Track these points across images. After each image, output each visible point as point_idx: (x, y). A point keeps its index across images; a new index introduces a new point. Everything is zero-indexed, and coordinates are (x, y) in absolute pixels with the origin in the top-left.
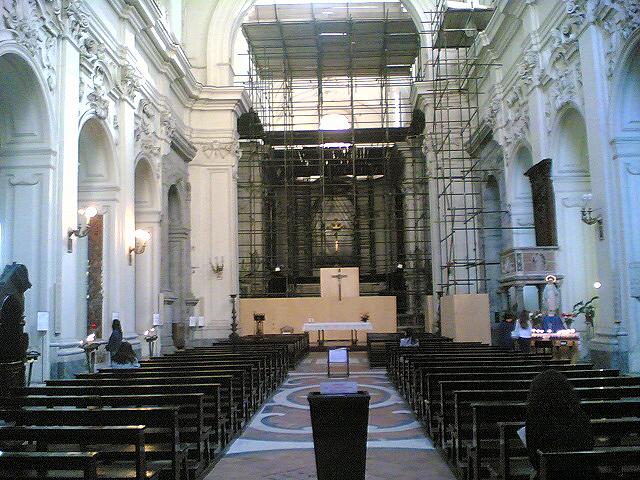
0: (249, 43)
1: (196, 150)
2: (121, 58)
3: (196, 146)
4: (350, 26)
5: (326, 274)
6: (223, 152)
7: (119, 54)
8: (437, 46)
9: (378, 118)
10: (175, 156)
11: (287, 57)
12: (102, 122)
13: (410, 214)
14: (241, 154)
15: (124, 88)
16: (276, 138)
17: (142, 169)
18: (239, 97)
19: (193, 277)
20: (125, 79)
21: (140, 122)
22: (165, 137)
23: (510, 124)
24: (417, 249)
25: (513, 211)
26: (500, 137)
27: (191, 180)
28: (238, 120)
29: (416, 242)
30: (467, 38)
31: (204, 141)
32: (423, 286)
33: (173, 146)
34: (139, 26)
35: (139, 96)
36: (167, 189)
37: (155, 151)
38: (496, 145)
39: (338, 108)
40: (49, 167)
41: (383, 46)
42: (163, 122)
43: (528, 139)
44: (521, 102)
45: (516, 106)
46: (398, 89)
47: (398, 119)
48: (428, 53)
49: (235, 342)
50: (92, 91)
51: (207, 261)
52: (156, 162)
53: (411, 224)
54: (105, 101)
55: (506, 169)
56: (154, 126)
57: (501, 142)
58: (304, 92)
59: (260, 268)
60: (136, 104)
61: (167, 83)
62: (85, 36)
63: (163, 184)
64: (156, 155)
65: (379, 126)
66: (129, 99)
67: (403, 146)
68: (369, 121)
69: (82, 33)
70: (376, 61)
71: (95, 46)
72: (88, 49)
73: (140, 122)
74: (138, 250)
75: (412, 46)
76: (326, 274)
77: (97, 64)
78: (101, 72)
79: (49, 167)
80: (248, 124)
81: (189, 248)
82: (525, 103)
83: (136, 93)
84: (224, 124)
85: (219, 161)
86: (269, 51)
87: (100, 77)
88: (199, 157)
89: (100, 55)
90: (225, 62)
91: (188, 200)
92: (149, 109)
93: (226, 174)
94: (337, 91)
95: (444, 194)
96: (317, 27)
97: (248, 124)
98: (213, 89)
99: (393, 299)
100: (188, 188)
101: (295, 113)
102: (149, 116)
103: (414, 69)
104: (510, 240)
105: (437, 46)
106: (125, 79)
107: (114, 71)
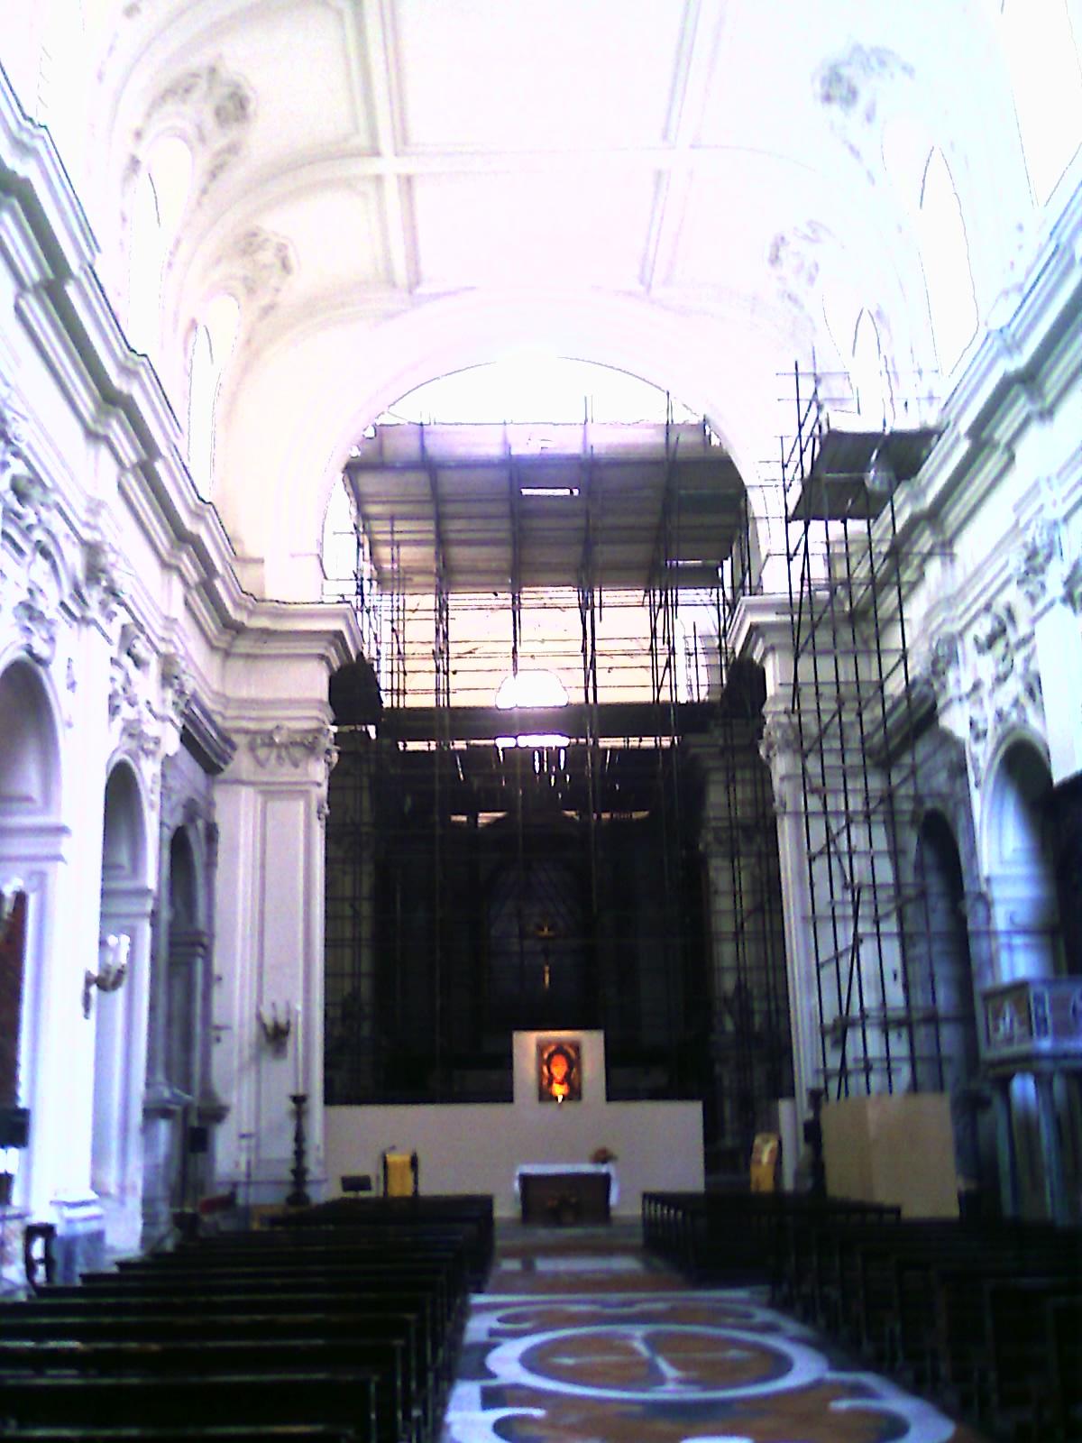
0: (359, 509)
1: (233, 747)
2: (87, 525)
3: (236, 738)
4: (589, 471)
5: (686, 1117)
6: (298, 753)
7: (85, 517)
8: (806, 511)
9: (646, 677)
10: (188, 763)
11: (441, 542)
12: (41, 670)
13: (723, 903)
14: (335, 758)
15: (94, 596)
16: (419, 722)
17: (121, 786)
18: (338, 625)
19: (217, 1053)
20: (95, 572)
21: (119, 676)
22: (172, 714)
23: (984, 692)
24: (740, 987)
25: (998, 892)
26: (955, 721)
27: (221, 818)
28: (331, 680)
29: (740, 968)
30: (869, 496)
31: (252, 726)
32: (759, 1075)
33: (186, 739)
34: (130, 455)
35: (123, 617)
36: (168, 834)
37: (151, 746)
38: (947, 739)
39: (530, 664)
40: (58, 858)
41: (666, 514)
42: (167, 678)
43: (1034, 722)
44: (1013, 637)
45: (999, 648)
46: (696, 614)
47: (693, 682)
48: (771, 531)
49: (298, 1210)
50: (25, 596)
51: (249, 1013)
52: (148, 772)
53: (725, 925)
54: (51, 622)
55: (976, 796)
56: (147, 685)
57: (961, 730)
58: (478, 618)
59: (366, 1029)
60: (114, 631)
61: (178, 589)
62: (17, 467)
63: (162, 824)
64: (148, 753)
65: (646, 696)
66: (102, 621)
67: (707, 744)
68: (625, 685)
69: (10, 458)
70: (640, 552)
71: (36, 492)
72: (22, 496)
73: (119, 676)
74: (106, 981)
75: (728, 519)
76: (686, 1117)
77: (38, 535)
78: (46, 554)
79: (58, 858)
80: (353, 686)
81: (210, 979)
82: (1024, 641)
83: (114, 607)
84: (304, 686)
85: (287, 774)
86: (399, 526)
87: (42, 564)
88: (242, 763)
89: (44, 513)
90: (302, 549)
91: (211, 864)
92: (141, 648)
93: (301, 805)
94: (552, 615)
95: (827, 852)
96: (517, 471)
97: (353, 686)
98: (280, 609)
99: (691, 1113)
100: (211, 834)
101: (453, 665)
102: (138, 662)
103: (726, 572)
104: (992, 962)
105: (806, 511)
106: (95, 572)
107: (74, 559)
